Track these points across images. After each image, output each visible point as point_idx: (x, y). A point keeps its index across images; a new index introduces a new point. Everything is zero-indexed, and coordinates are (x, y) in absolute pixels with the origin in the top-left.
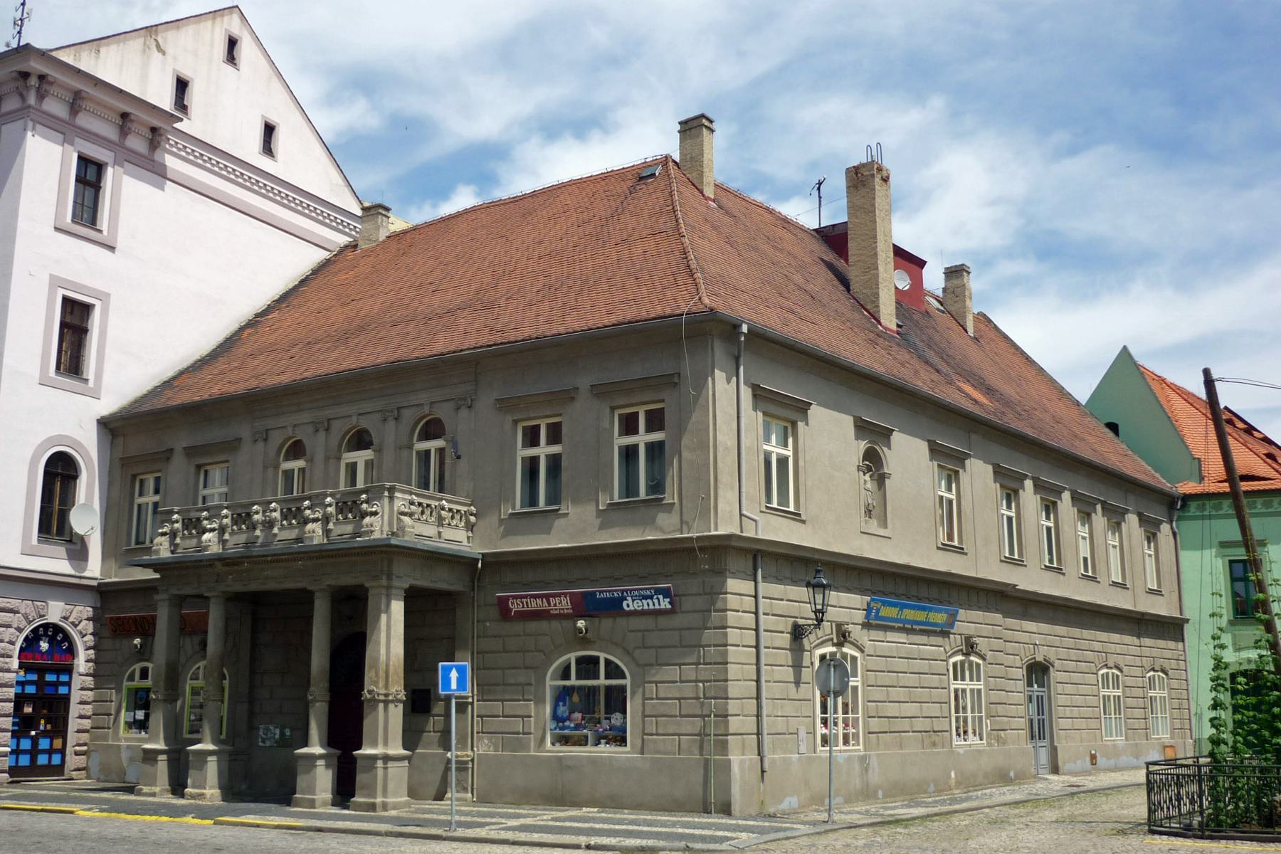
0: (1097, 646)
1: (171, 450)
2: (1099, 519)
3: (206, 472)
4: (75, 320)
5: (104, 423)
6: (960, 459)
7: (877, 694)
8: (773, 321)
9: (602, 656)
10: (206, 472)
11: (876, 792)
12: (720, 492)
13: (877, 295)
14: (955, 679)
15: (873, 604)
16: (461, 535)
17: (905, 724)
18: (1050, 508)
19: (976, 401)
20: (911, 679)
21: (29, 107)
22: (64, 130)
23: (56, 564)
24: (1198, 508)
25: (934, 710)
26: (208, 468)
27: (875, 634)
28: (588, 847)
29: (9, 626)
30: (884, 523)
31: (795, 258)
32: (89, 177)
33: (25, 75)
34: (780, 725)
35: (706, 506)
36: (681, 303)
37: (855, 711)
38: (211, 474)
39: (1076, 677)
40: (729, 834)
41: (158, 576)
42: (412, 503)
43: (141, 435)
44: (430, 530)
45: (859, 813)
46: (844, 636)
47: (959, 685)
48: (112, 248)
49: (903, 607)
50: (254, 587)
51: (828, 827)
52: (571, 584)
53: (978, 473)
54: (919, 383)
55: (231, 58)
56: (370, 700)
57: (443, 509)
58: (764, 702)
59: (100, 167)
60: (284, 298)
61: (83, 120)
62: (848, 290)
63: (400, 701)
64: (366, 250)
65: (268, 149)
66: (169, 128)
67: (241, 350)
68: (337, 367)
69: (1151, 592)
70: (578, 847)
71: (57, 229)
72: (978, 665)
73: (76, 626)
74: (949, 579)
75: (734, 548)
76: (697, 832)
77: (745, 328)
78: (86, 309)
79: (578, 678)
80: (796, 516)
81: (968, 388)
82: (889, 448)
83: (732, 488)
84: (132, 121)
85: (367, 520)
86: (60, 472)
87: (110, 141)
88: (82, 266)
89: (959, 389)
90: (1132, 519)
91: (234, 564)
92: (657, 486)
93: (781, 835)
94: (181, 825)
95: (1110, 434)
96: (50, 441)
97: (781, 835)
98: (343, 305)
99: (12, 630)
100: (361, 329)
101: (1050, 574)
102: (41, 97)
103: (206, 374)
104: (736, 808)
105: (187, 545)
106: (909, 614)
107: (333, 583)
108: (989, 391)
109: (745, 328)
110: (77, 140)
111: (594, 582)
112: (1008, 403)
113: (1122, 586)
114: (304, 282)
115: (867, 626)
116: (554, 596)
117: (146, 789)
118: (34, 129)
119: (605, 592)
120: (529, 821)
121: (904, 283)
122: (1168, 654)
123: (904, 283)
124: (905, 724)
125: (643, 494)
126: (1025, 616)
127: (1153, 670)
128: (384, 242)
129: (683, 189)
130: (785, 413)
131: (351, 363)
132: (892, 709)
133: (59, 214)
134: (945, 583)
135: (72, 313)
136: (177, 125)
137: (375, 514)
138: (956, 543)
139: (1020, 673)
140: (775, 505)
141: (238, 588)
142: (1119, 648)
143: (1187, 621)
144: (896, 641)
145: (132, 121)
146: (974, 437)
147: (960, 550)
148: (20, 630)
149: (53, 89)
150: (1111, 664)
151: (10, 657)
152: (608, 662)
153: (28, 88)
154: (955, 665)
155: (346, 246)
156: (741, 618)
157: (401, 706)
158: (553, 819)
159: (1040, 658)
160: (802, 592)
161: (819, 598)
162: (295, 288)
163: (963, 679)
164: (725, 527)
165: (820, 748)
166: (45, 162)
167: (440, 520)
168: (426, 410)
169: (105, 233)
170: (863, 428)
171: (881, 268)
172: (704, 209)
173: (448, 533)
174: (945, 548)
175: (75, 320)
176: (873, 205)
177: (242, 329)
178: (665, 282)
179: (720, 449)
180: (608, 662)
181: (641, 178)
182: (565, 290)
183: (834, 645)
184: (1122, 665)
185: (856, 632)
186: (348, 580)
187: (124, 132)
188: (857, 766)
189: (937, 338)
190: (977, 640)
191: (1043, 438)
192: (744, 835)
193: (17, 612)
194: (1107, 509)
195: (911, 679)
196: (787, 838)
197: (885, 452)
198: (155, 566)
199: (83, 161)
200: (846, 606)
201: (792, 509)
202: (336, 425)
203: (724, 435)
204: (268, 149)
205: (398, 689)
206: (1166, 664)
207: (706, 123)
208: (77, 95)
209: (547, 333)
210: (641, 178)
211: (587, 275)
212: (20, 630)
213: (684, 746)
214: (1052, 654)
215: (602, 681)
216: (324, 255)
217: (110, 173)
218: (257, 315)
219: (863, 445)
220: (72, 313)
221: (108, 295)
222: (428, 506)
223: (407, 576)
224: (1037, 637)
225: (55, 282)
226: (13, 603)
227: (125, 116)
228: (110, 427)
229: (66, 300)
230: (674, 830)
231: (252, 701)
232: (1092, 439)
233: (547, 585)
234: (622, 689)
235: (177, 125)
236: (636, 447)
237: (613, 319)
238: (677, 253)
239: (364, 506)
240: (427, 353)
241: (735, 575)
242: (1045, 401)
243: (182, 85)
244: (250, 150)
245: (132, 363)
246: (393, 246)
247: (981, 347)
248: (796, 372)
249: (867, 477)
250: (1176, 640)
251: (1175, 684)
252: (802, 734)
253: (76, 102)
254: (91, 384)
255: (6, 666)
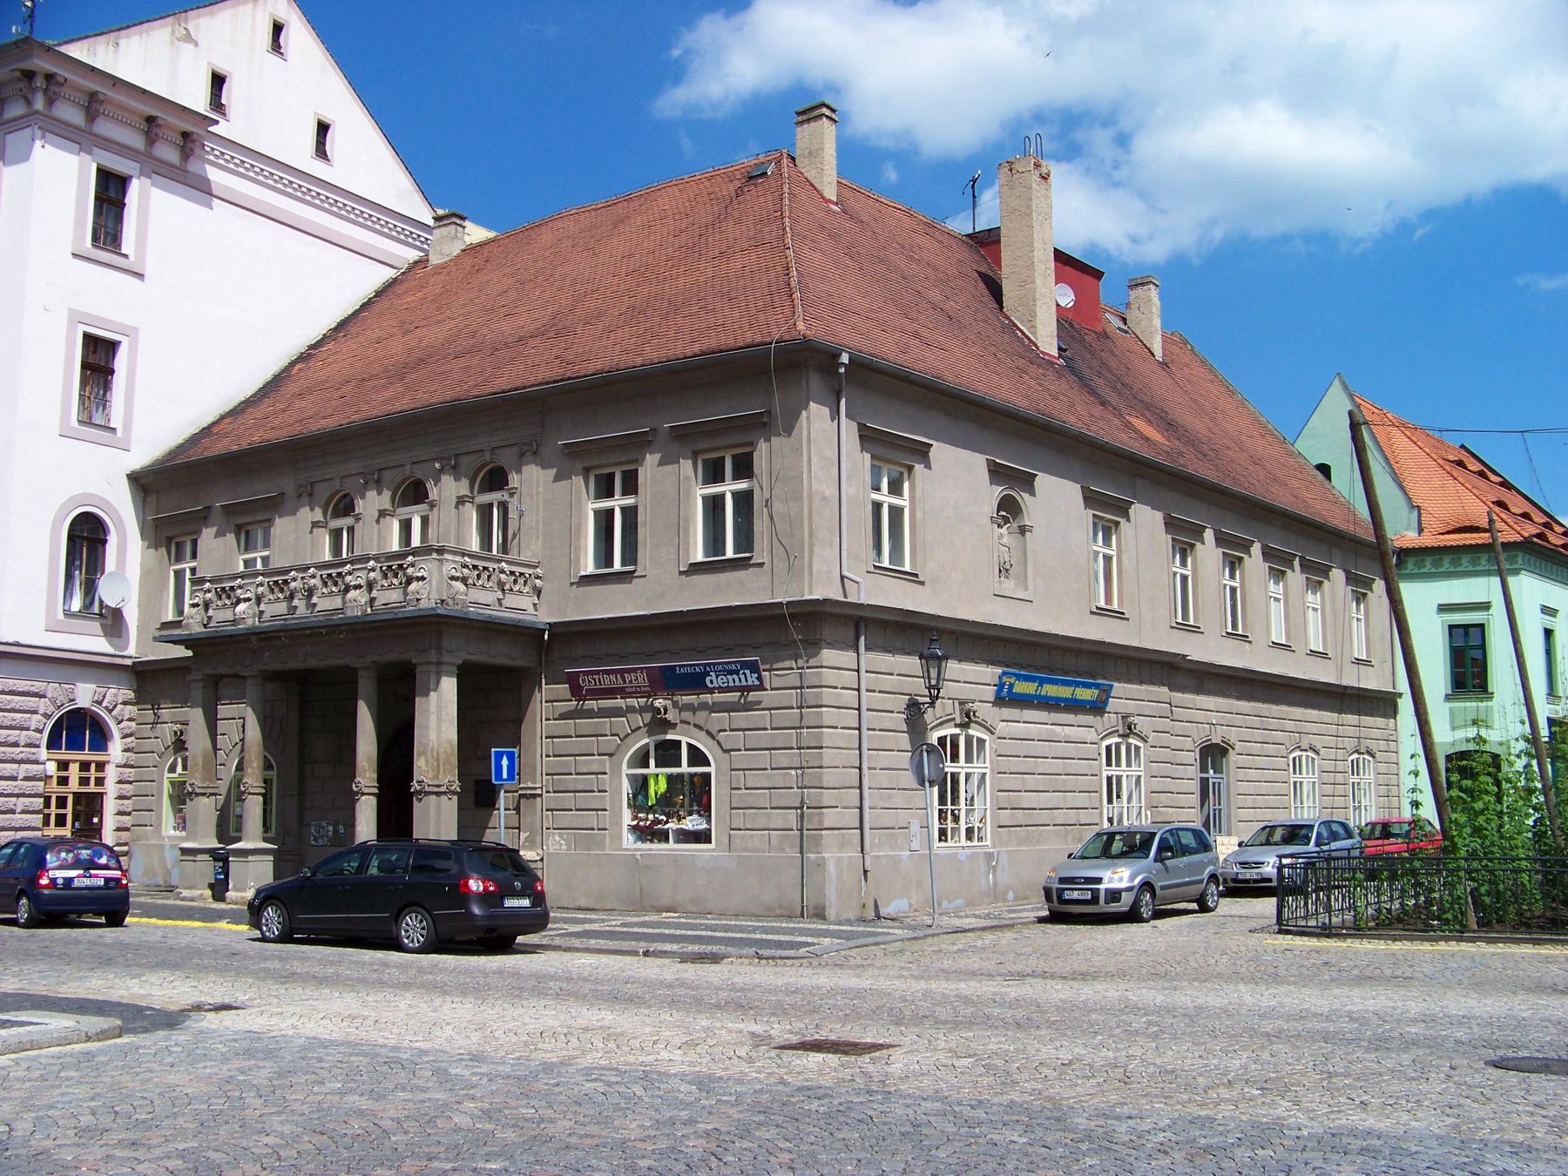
0: (1289, 725)
1: (208, 508)
2: (1296, 577)
3: (247, 533)
4: (98, 359)
5: (135, 479)
6: (1123, 509)
7: (1010, 782)
8: (887, 347)
9: (684, 740)
10: (247, 533)
11: (1005, 893)
12: (816, 550)
13: (1033, 315)
14: (1109, 764)
15: (1005, 679)
16: (526, 602)
17: (1044, 817)
18: (1233, 564)
19: (1147, 439)
20: (1056, 766)
21: (37, 112)
22: (78, 138)
23: (93, 642)
24: (1452, 563)
25: (1081, 800)
26: (250, 528)
27: (1008, 712)
28: (646, 954)
29: (35, 712)
30: (1023, 582)
31: (935, 269)
32: (110, 194)
33: (29, 75)
34: (888, 818)
35: (794, 562)
36: (772, 329)
37: (955, 800)
38: (252, 534)
39: (1261, 762)
40: (810, 940)
41: (190, 653)
42: (465, 566)
43: (194, 490)
44: (490, 597)
45: (976, 916)
46: (968, 716)
47: (1113, 771)
48: (140, 276)
49: (1042, 682)
50: (293, 664)
51: (929, 931)
52: (650, 657)
53: (1146, 521)
54: (1072, 419)
55: (276, 47)
56: (419, 792)
57: (502, 572)
58: (866, 791)
59: (123, 182)
60: (343, 325)
61: (104, 127)
62: (1001, 307)
63: (454, 793)
64: (437, 266)
65: (321, 152)
66: (202, 133)
67: (290, 388)
68: (390, 408)
69: (1358, 661)
70: (634, 953)
71: (75, 255)
72: (1137, 748)
73: (110, 711)
74: (1102, 649)
75: (831, 615)
76: (782, 938)
77: (845, 358)
78: (113, 346)
79: (690, 765)
80: (912, 577)
81: (1139, 424)
82: (1032, 493)
83: (831, 545)
84: (159, 126)
85: (413, 586)
86: (87, 538)
87: (137, 152)
88: (105, 297)
89: (1129, 425)
90: (1337, 575)
91: (272, 638)
92: (745, 539)
93: (871, 940)
94: (211, 930)
95: (1320, 476)
96: (87, 497)
97: (871, 940)
98: (407, 332)
99: (38, 717)
100: (421, 361)
101: (1232, 642)
102: (50, 102)
103: (249, 419)
104: (831, 913)
105: (220, 615)
106: (1051, 690)
107: (378, 658)
108: (1169, 425)
109: (845, 358)
110: (96, 150)
111: (675, 654)
112: (1191, 441)
113: (1323, 655)
114: (365, 306)
115: (999, 701)
116: (629, 671)
117: (186, 893)
118: (43, 137)
119: (687, 665)
120: (595, 927)
121: (1067, 298)
122: (1375, 733)
123: (1067, 298)
124: (1044, 817)
125: (730, 553)
126: (1199, 690)
127: (1357, 751)
128: (458, 256)
129: (797, 190)
130: (895, 455)
131: (404, 404)
132: (1028, 799)
133: (78, 238)
134: (1097, 654)
135: (95, 352)
136: (212, 129)
137: (423, 578)
138: (1115, 606)
139: (1193, 757)
140: (886, 564)
141: (277, 666)
142: (1314, 728)
143: (1400, 695)
144: (1033, 723)
145: (159, 126)
146: (1139, 483)
147: (1120, 615)
148: (47, 716)
149: (63, 91)
150: (1305, 745)
151: (38, 746)
152: (690, 746)
153: (34, 90)
154: (1108, 748)
155: (416, 262)
156: (840, 695)
157: (455, 798)
158: (623, 925)
159: (1216, 740)
160: (912, 663)
161: (934, 673)
162: (356, 313)
163: (1118, 764)
164: (823, 589)
165: (937, 844)
166: (57, 176)
167: (501, 585)
168: (488, 456)
169: (131, 257)
170: (997, 473)
171: (1039, 282)
172: (819, 214)
173: (510, 600)
174: (1100, 612)
175: (98, 359)
176: (1029, 207)
177: (292, 364)
178: (760, 303)
179: (817, 499)
180: (690, 746)
181: (751, 178)
182: (650, 313)
183: (956, 726)
184: (1318, 747)
185: (985, 711)
186: (393, 656)
187: (151, 141)
188: (982, 863)
189: (1112, 363)
190: (1136, 719)
191: (1227, 484)
192: (827, 941)
193: (44, 696)
194: (1307, 566)
195: (1056, 766)
196: (877, 944)
197: (1024, 498)
198: (187, 642)
199: (104, 176)
200: (971, 679)
201: (907, 568)
202: (387, 475)
203: (820, 482)
204: (321, 152)
205: (450, 777)
206: (1373, 745)
207: (828, 112)
208: (93, 96)
209: (622, 366)
210: (751, 178)
211: (676, 295)
212: (47, 716)
213: (774, 842)
214: (1232, 735)
215: (685, 768)
216: (390, 274)
217: (135, 188)
218: (311, 347)
219: (998, 491)
220: (95, 352)
221: (136, 330)
222: (485, 568)
223: (462, 650)
224: (1212, 713)
225: (76, 317)
226: (38, 686)
227: (150, 120)
228: (142, 483)
229: (87, 336)
230: (752, 936)
231: (302, 795)
232: (1296, 484)
233: (623, 658)
234: (708, 775)
235: (212, 129)
236: (722, 496)
237: (696, 348)
238: (779, 269)
239: (410, 570)
240: (488, 389)
241: (831, 646)
242: (1244, 438)
243: (218, 81)
244: (300, 154)
245: (170, 403)
246: (468, 261)
247: (1170, 374)
248: (905, 408)
249: (1004, 530)
250: (1385, 716)
251: (1383, 768)
252: (915, 827)
253: (93, 105)
254: (119, 433)
255: (33, 757)
